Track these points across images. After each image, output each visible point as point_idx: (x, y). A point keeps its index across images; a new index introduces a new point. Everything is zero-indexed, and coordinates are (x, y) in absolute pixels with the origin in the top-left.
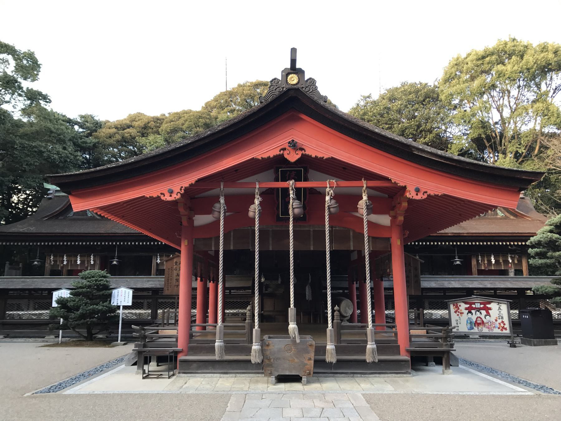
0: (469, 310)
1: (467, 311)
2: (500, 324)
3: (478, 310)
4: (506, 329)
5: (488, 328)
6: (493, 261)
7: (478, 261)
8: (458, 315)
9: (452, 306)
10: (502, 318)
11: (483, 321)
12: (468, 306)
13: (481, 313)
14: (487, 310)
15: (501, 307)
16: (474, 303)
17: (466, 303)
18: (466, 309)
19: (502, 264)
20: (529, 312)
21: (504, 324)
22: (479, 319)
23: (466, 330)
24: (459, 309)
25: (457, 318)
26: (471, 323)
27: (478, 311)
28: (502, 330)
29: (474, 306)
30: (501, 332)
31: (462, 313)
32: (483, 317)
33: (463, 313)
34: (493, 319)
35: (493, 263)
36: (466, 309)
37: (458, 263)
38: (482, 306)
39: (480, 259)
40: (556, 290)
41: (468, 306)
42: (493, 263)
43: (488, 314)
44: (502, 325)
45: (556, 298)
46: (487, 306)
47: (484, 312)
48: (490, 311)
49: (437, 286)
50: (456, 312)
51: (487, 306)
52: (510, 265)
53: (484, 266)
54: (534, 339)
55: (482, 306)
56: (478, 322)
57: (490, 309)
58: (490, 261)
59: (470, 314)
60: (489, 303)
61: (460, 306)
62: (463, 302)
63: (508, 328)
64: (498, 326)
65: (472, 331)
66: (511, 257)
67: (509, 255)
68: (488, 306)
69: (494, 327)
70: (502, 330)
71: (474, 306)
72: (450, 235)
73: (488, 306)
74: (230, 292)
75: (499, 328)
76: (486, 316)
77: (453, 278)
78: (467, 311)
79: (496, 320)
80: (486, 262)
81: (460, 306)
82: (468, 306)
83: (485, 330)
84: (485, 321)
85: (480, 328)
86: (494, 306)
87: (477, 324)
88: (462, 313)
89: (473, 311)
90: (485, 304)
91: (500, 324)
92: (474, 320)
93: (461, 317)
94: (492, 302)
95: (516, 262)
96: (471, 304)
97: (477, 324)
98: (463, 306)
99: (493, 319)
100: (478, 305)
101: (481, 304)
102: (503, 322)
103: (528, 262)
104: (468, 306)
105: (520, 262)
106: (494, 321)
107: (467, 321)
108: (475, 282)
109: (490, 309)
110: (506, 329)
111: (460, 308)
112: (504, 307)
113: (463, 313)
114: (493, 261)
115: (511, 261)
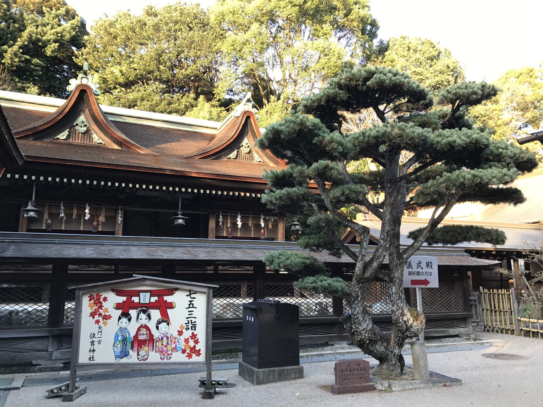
0: (124, 311)
1: (120, 311)
2: (187, 341)
3: (145, 308)
4: (198, 353)
5: (161, 352)
6: (239, 224)
7: (217, 223)
8: (97, 322)
9: (86, 301)
10: (194, 327)
11: (151, 336)
12: (124, 299)
13: (149, 317)
14: (164, 307)
15: (195, 302)
16: (137, 294)
17: (119, 293)
18: (118, 306)
19: (252, 229)
20: (487, 160)
21: (197, 342)
22: (143, 331)
23: (112, 359)
24: (101, 307)
25: (95, 329)
26: (124, 340)
27: (144, 312)
28: (190, 356)
29: (136, 299)
30: (187, 360)
31: (107, 318)
32: (152, 325)
33: (109, 317)
34: (172, 330)
35: (239, 226)
36: (118, 306)
37: (180, 221)
38: (154, 299)
39: (221, 220)
40: (308, 261)
41: (124, 299)
42: (239, 226)
43: (165, 319)
44: (192, 343)
45: (306, 280)
46: (165, 298)
47: (156, 314)
48: (169, 311)
49: (95, 256)
50: (93, 315)
51: (165, 298)
52: (262, 231)
53: (227, 231)
54: (259, 367)
55: (154, 299)
56: (141, 338)
57: (171, 306)
58: (235, 224)
59: (124, 320)
60: (171, 292)
61: (105, 299)
62: (113, 290)
63: (203, 352)
64: (182, 345)
65: (125, 360)
66: (265, 220)
67: (262, 217)
68: (168, 299)
69: (175, 349)
70: (190, 356)
71: (136, 299)
72: (168, 172)
73: (168, 299)
74: (216, 269)
75: (184, 351)
76: (159, 323)
77: (137, 240)
78: (120, 311)
79: (180, 333)
80: (229, 225)
81: (105, 299)
82: (122, 299)
83: (154, 357)
84: (156, 334)
85: (142, 353)
86: (179, 299)
87: (138, 343)
88: (107, 318)
89: (133, 313)
90: (160, 294)
91: (187, 341)
92: (133, 334)
93: (104, 328)
94: (177, 289)
95: (270, 226)
96: (130, 294)
97: (138, 343)
98: (112, 300)
99: (172, 330)
100: (145, 298)
101: (153, 293)
102: (194, 336)
103: (386, 348)
104: (122, 299)
105: (275, 226)
106: (176, 334)
107: (117, 336)
108: (179, 249)
109: (171, 306)
110: (198, 353)
111: (104, 304)
112: (200, 300)
113: (109, 317)
114: (239, 224)
115: (263, 225)
